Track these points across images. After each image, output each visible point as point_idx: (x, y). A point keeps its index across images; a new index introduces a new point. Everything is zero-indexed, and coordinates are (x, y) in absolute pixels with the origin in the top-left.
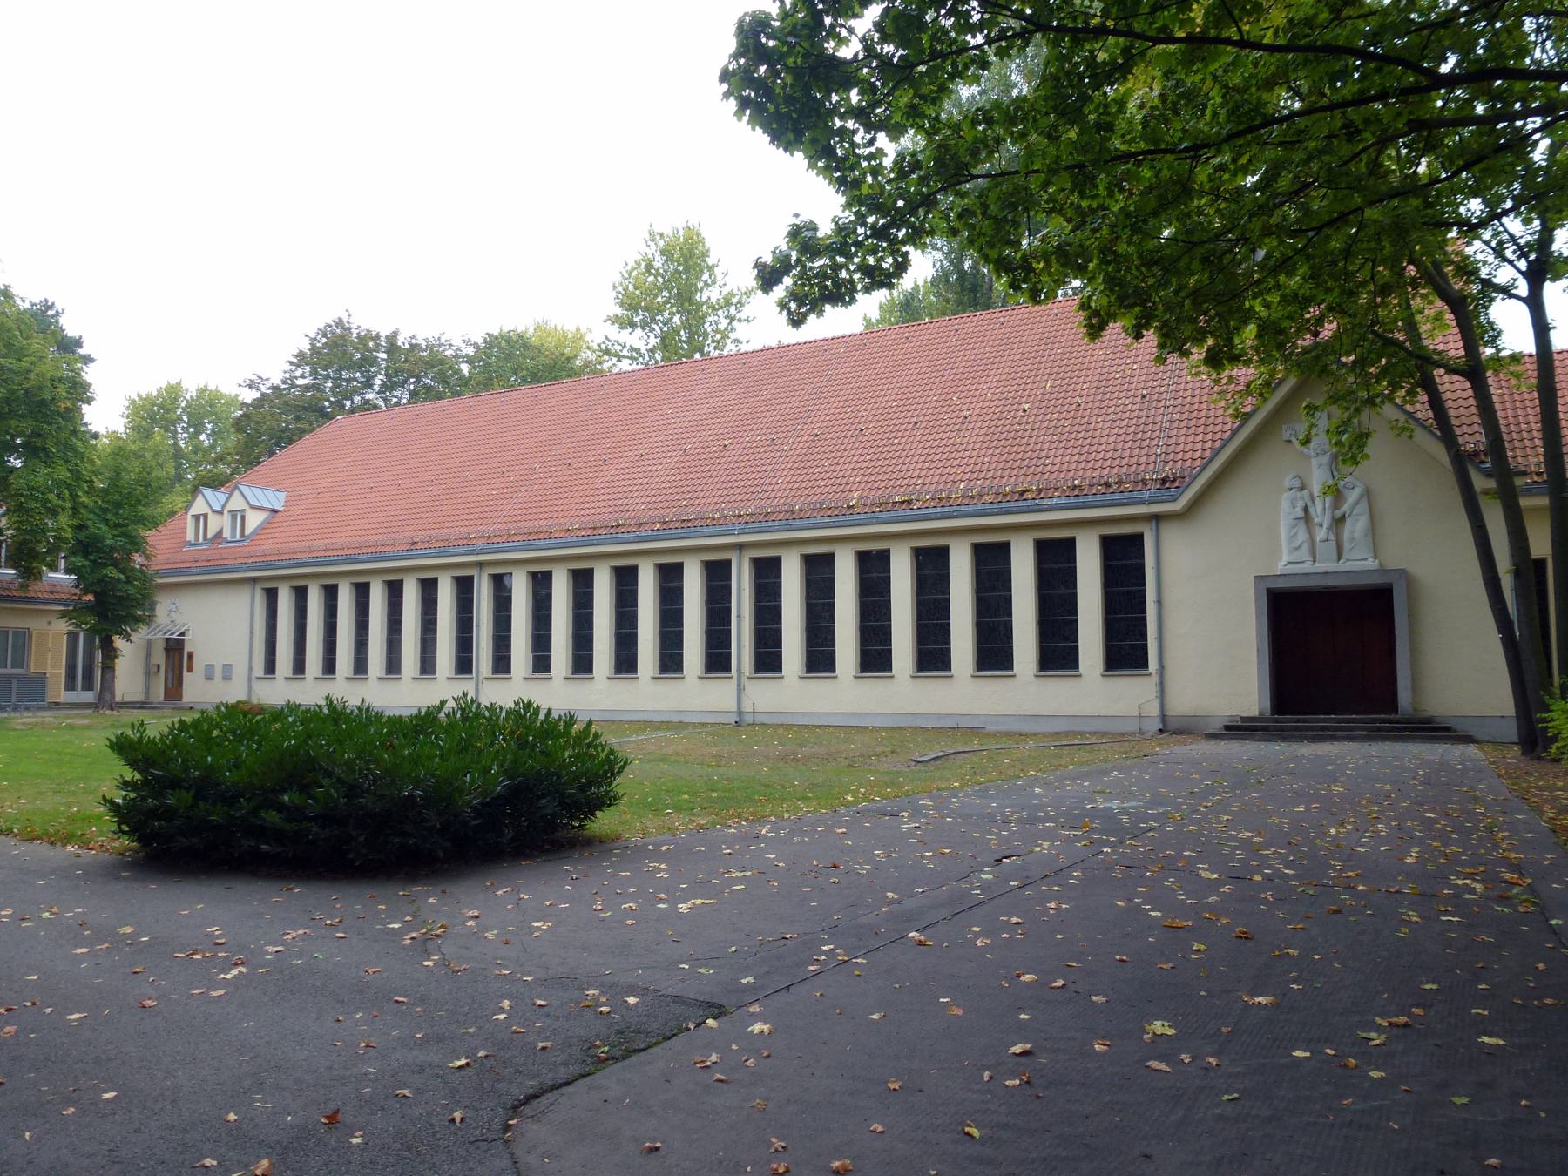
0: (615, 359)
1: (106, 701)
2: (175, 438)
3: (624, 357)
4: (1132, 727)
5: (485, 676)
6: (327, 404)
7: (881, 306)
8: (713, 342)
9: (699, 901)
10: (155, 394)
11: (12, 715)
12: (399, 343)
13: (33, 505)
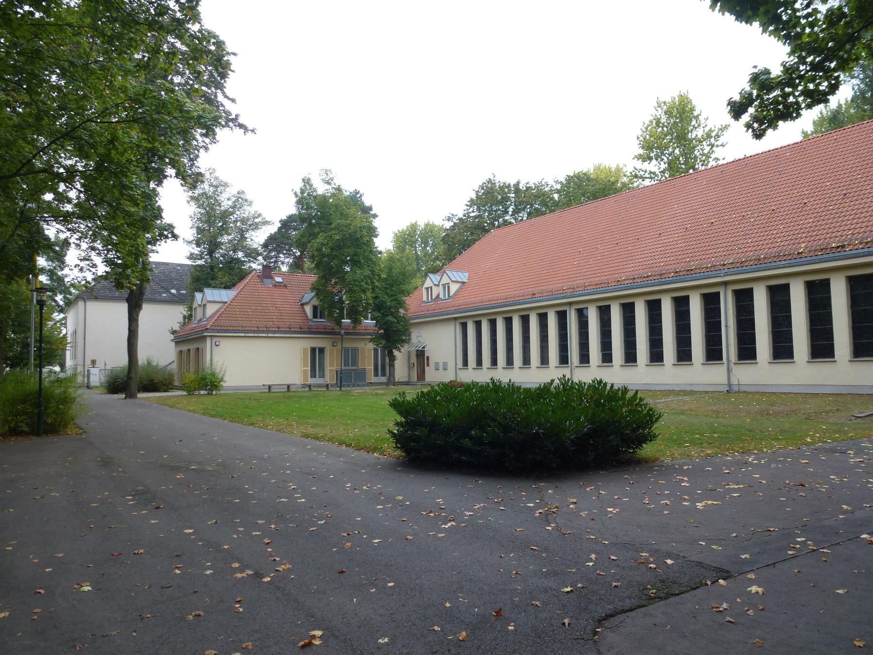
0: (640, 180)
1: (391, 382)
2: (416, 250)
3: (646, 178)
5: (576, 365)
6: (486, 225)
7: (814, 122)
8: (701, 161)
9: (710, 502)
10: (405, 229)
11: (353, 388)
12: (521, 188)
13: (356, 288)
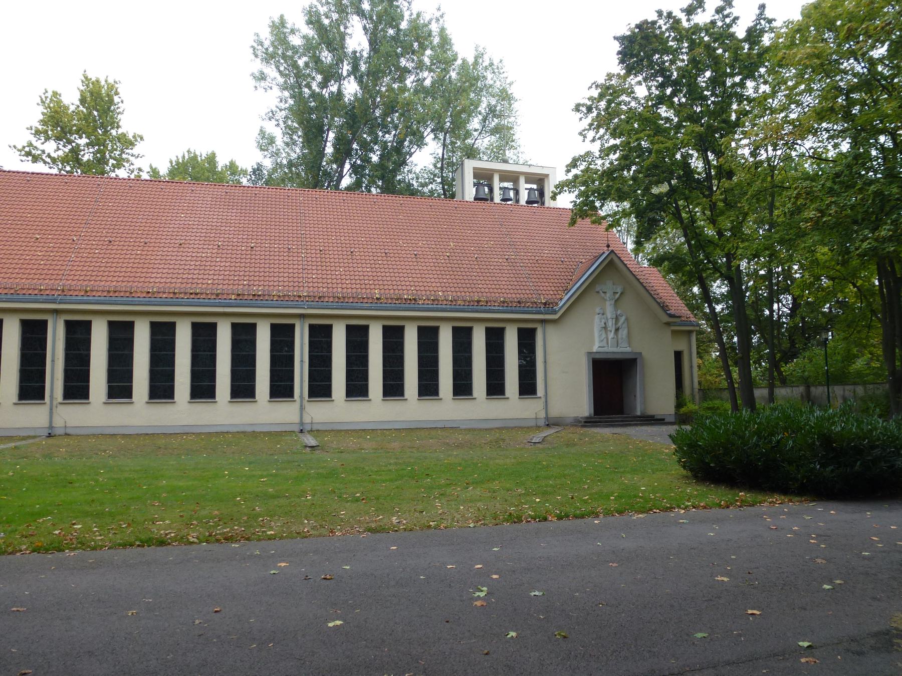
4: (533, 423)
